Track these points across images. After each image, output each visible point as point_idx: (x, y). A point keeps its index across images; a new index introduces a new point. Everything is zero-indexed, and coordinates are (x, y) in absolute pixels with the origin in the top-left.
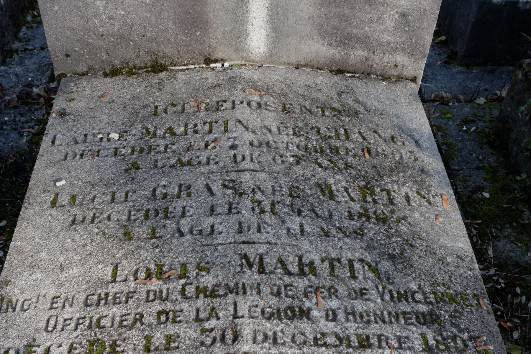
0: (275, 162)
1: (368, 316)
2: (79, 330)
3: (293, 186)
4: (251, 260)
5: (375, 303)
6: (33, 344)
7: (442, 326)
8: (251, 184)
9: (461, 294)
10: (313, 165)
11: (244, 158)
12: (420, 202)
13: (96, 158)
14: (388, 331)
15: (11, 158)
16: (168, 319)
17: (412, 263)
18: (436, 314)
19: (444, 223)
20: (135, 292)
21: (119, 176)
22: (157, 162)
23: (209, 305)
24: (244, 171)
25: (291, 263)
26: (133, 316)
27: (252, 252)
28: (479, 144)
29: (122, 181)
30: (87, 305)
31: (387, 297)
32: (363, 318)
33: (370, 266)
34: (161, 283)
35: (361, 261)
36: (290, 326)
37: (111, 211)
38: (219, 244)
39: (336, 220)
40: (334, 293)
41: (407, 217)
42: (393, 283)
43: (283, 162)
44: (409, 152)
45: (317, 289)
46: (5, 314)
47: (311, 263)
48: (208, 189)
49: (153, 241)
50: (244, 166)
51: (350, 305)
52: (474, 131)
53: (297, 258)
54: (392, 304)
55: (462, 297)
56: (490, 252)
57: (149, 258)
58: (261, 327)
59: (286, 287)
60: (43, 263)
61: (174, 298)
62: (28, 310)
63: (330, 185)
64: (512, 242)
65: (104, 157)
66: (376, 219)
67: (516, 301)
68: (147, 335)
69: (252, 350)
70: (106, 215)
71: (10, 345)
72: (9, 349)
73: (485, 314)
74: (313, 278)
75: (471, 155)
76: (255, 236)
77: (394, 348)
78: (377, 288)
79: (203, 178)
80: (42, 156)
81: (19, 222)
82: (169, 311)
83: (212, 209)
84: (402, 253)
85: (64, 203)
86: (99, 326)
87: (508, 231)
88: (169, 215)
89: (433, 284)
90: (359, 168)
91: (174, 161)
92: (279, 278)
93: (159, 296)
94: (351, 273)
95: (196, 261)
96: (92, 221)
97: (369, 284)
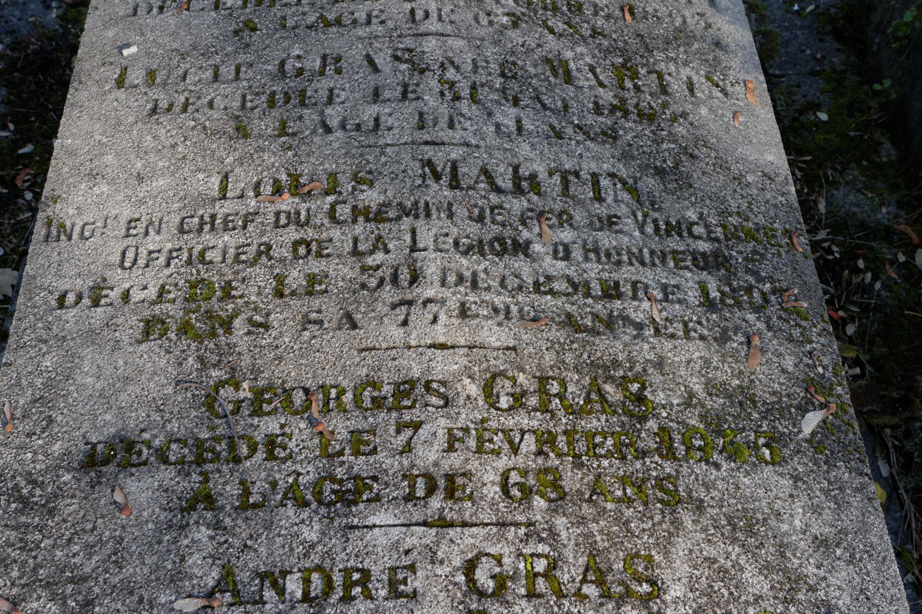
0: (478, 23)
1: (619, 254)
2: (172, 266)
3: (507, 61)
4: (439, 169)
5: (630, 236)
6: (102, 285)
7: (731, 273)
8: (439, 55)
9: (764, 228)
10: (540, 29)
11: (427, 15)
12: (710, 92)
13: (185, 12)
14: (648, 276)
15: (33, 44)
18: (724, 256)
19: (746, 124)
20: (257, 213)
21: (225, 41)
22: (285, 20)
23: (372, 233)
24: (427, 35)
25: (501, 175)
26: (254, 247)
27: (439, 156)
28: (818, 33)
29: (229, 49)
30: (182, 231)
31: (649, 229)
32: (612, 258)
33: (624, 183)
34: (297, 200)
35: (612, 175)
36: (497, 264)
37: (213, 95)
38: (388, 145)
39: (574, 114)
40: (567, 221)
41: (688, 114)
43: (491, 23)
44: (698, 14)
45: (541, 214)
46: (55, 244)
47: (533, 177)
48: (369, 62)
49: (283, 139)
50: (427, 28)
51: (591, 238)
52: (812, 11)
53: (511, 169)
54: (657, 238)
55: (765, 233)
56: (822, 207)
57: (277, 164)
58: (453, 265)
59: (492, 209)
60: (110, 171)
61: (318, 222)
62: (91, 237)
63: (566, 62)
64: (859, 191)
65: (199, 11)
66: (639, 115)
67: (856, 280)
68: (278, 274)
69: (440, 295)
70: (205, 101)
71: (67, 287)
72: (66, 292)
73: (799, 258)
74: (535, 198)
75: (803, 51)
76: (444, 134)
77: (656, 300)
78: (635, 216)
79: (360, 46)
80: (96, 8)
81: (66, 110)
82: (311, 241)
83: (376, 93)
84: (676, 166)
85: (136, 82)
86: (202, 261)
87: (853, 173)
88: (307, 101)
89: (723, 213)
90: (614, 36)
91: (313, 19)
92: (481, 196)
93: (294, 219)
94: (594, 193)
95: (351, 169)
96: (185, 110)
97: (623, 210)
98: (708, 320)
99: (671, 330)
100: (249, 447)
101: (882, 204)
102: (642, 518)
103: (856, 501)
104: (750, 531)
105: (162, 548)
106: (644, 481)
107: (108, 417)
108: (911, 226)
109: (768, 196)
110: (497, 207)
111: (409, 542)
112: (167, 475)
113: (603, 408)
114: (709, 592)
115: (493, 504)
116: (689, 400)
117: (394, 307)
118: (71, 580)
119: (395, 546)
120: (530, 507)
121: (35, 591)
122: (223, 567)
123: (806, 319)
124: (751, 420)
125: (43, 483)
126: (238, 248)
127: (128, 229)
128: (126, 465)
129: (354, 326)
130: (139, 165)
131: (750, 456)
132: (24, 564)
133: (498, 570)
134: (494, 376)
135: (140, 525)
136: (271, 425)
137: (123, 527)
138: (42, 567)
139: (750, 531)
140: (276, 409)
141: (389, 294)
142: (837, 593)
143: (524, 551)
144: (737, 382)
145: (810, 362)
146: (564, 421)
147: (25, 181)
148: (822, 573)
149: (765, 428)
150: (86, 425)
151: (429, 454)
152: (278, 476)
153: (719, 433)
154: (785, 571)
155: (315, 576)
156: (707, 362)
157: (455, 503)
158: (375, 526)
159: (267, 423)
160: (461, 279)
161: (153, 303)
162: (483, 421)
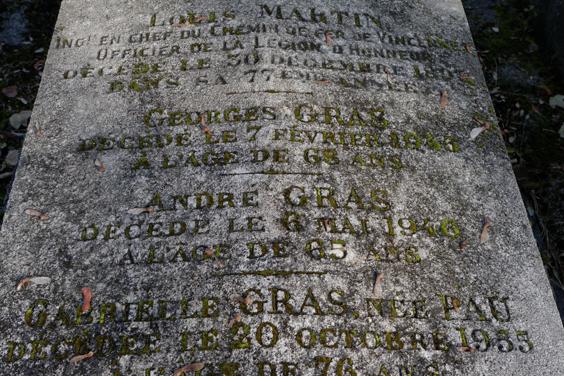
2: (126, 57)
4: (271, 9)
5: (376, 43)
14: (385, 62)
16: (200, 49)
17: (410, 19)
18: (428, 54)
23: (234, 39)
25: (305, 13)
26: (170, 48)
31: (387, 40)
33: (373, 19)
34: (193, 25)
35: (366, 15)
40: (341, 36)
42: (392, 31)
45: (327, 31)
51: (354, 44)
53: (310, 10)
56: (495, 77)
58: (278, 54)
59: (300, 29)
61: (205, 35)
64: (517, 68)
67: (515, 114)
71: (69, 68)
72: (68, 71)
73: (470, 56)
77: (390, 73)
78: (379, 34)
82: (201, 44)
84: (402, 11)
89: (428, 34)
93: (192, 34)
97: (372, 31)
98: (419, 84)
99: (398, 88)
100: (168, 140)
102: (381, 173)
103: (500, 170)
104: (441, 181)
106: (382, 157)
107: (92, 128)
108: (547, 86)
109: (453, 27)
110: (302, 28)
111: (254, 181)
112: (123, 153)
113: (360, 123)
114: (418, 209)
115: (299, 164)
116: (408, 120)
117: (246, 73)
118: (73, 202)
119: (247, 183)
120: (320, 166)
121: (53, 207)
122: (154, 194)
123: (473, 85)
124: (442, 131)
125: (57, 158)
126: (161, 49)
127: (101, 42)
128: (100, 150)
129: (224, 83)
130: (107, 11)
131: (441, 147)
133: (302, 194)
134: (300, 106)
135: (109, 176)
136: (180, 130)
137: (100, 177)
138: (56, 196)
139: (441, 181)
140: (182, 122)
141: (243, 67)
142: (489, 212)
143: (316, 186)
144: (435, 113)
145: (476, 105)
146: (339, 128)
147: (39, 67)
148: (480, 202)
149: (450, 135)
150: (80, 132)
151: (265, 140)
152: (183, 153)
153: (424, 136)
154: (460, 201)
155: (204, 198)
156: (418, 103)
157: (279, 163)
158: (235, 174)
159: (177, 128)
160: (282, 61)
161: (116, 75)
162: (294, 127)
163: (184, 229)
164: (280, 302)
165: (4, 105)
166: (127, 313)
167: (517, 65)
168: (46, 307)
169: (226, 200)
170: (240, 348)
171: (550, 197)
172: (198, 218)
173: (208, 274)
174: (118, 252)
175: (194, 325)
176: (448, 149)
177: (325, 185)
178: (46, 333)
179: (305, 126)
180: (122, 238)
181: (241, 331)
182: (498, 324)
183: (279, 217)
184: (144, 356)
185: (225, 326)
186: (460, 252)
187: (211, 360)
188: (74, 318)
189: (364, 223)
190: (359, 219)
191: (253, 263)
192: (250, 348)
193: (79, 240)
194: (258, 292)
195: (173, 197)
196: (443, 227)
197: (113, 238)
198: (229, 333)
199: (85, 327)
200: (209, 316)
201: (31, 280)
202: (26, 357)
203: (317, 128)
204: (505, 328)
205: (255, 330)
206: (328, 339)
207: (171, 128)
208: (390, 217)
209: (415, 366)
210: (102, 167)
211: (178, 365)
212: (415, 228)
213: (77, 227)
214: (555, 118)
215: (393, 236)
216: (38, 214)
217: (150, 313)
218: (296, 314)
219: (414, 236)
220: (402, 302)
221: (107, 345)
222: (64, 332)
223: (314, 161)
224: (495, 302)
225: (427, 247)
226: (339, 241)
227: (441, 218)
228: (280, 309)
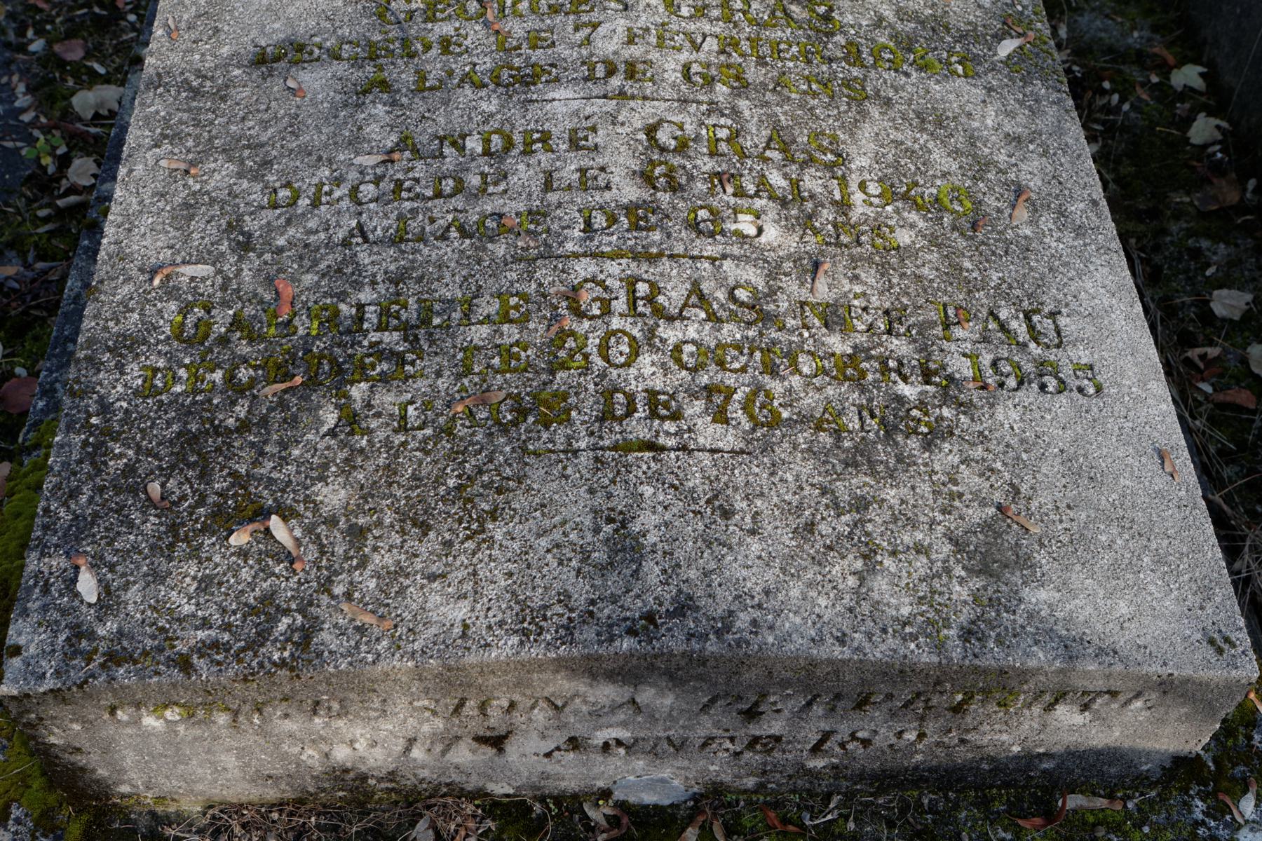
64: (1107, 16)
100: (424, 45)
101: (1133, 28)
103: (1052, 111)
104: (939, 123)
105: (339, 121)
107: (276, 26)
108: (1167, 48)
112: (340, 68)
114: (896, 165)
115: (673, 85)
116: (879, 22)
118: (248, 147)
119: (576, 113)
132: (197, 137)
133: (679, 133)
135: (314, 103)
139: (939, 123)
140: (450, 16)
148: (1013, 160)
151: (609, 43)
152: (454, 66)
154: (975, 156)
155: (495, 138)
158: (554, 100)
162: (663, 25)
163: (459, 188)
164: (642, 299)
165: (57, 75)
166: (360, 319)
167: (1108, 11)
168: (209, 312)
169: (538, 140)
170: (569, 369)
171: (1167, 253)
172: (487, 169)
173: (508, 256)
174: (338, 225)
175: (484, 335)
176: (955, 72)
177: (723, 121)
178: (212, 352)
179: (683, 24)
180: (345, 204)
181: (571, 343)
182: (1039, 351)
183: (637, 168)
184: (395, 383)
185: (542, 336)
186: (972, 238)
187: (517, 387)
188: (262, 327)
189: (795, 185)
190: (786, 176)
191: (592, 240)
192: (587, 369)
193: (263, 208)
194: (601, 283)
195: (437, 137)
196: (941, 196)
197: (328, 203)
198: (549, 347)
199: (284, 341)
200: (511, 321)
201: (178, 270)
202: (178, 389)
203: (707, 28)
204: (1052, 358)
205: (597, 341)
206: (729, 359)
207: (430, 26)
208: (844, 177)
209: (887, 407)
210: (300, 89)
211: (457, 396)
212: (890, 195)
213: (258, 187)
214: (1182, 108)
215: (849, 206)
216: (183, 166)
217: (404, 318)
218: (671, 319)
219: (889, 208)
220: (865, 309)
221: (327, 368)
222: (244, 349)
223: (701, 81)
224: (1035, 318)
225: (912, 226)
226: (749, 211)
227: (938, 182)
228: (640, 309)
